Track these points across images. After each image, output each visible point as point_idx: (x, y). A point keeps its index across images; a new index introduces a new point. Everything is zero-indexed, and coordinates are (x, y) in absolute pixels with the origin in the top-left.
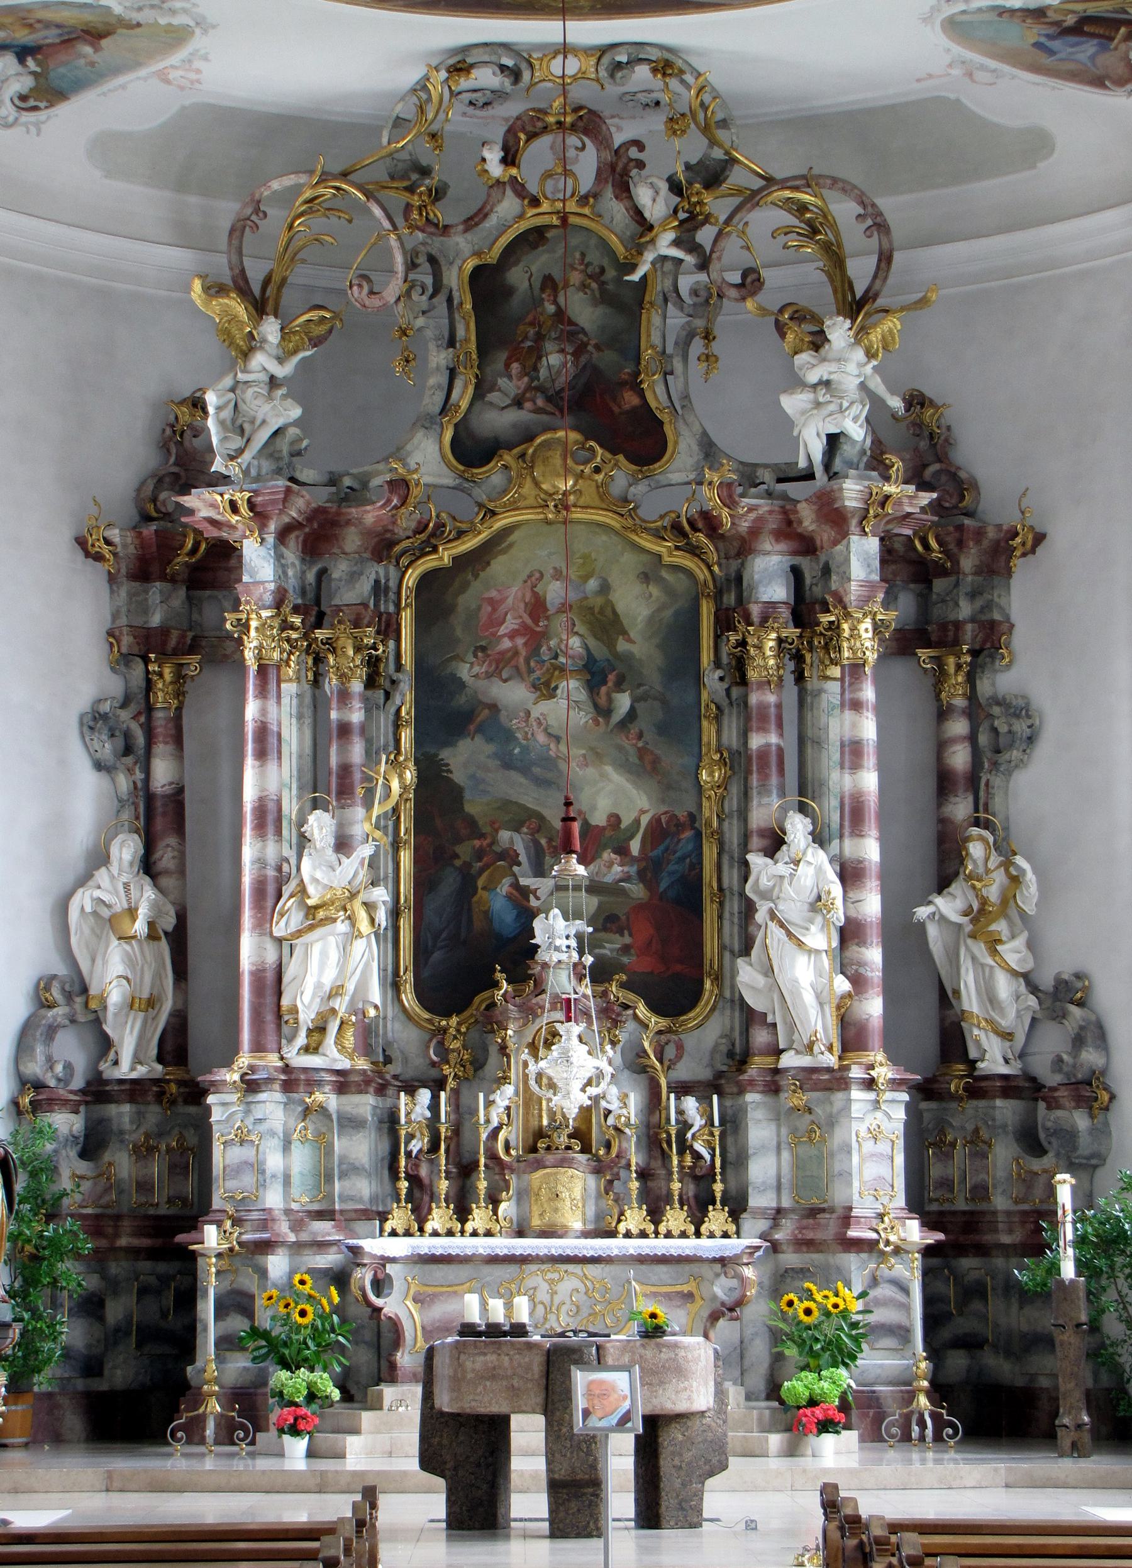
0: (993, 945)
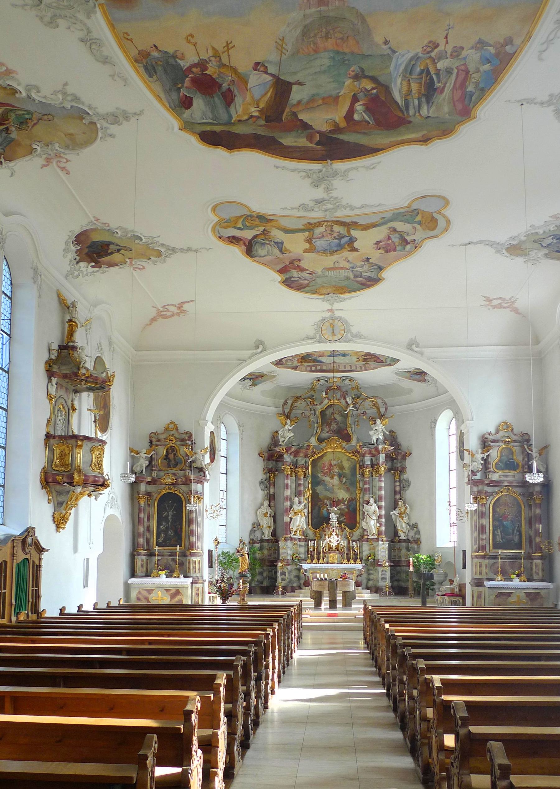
0: (402, 518)
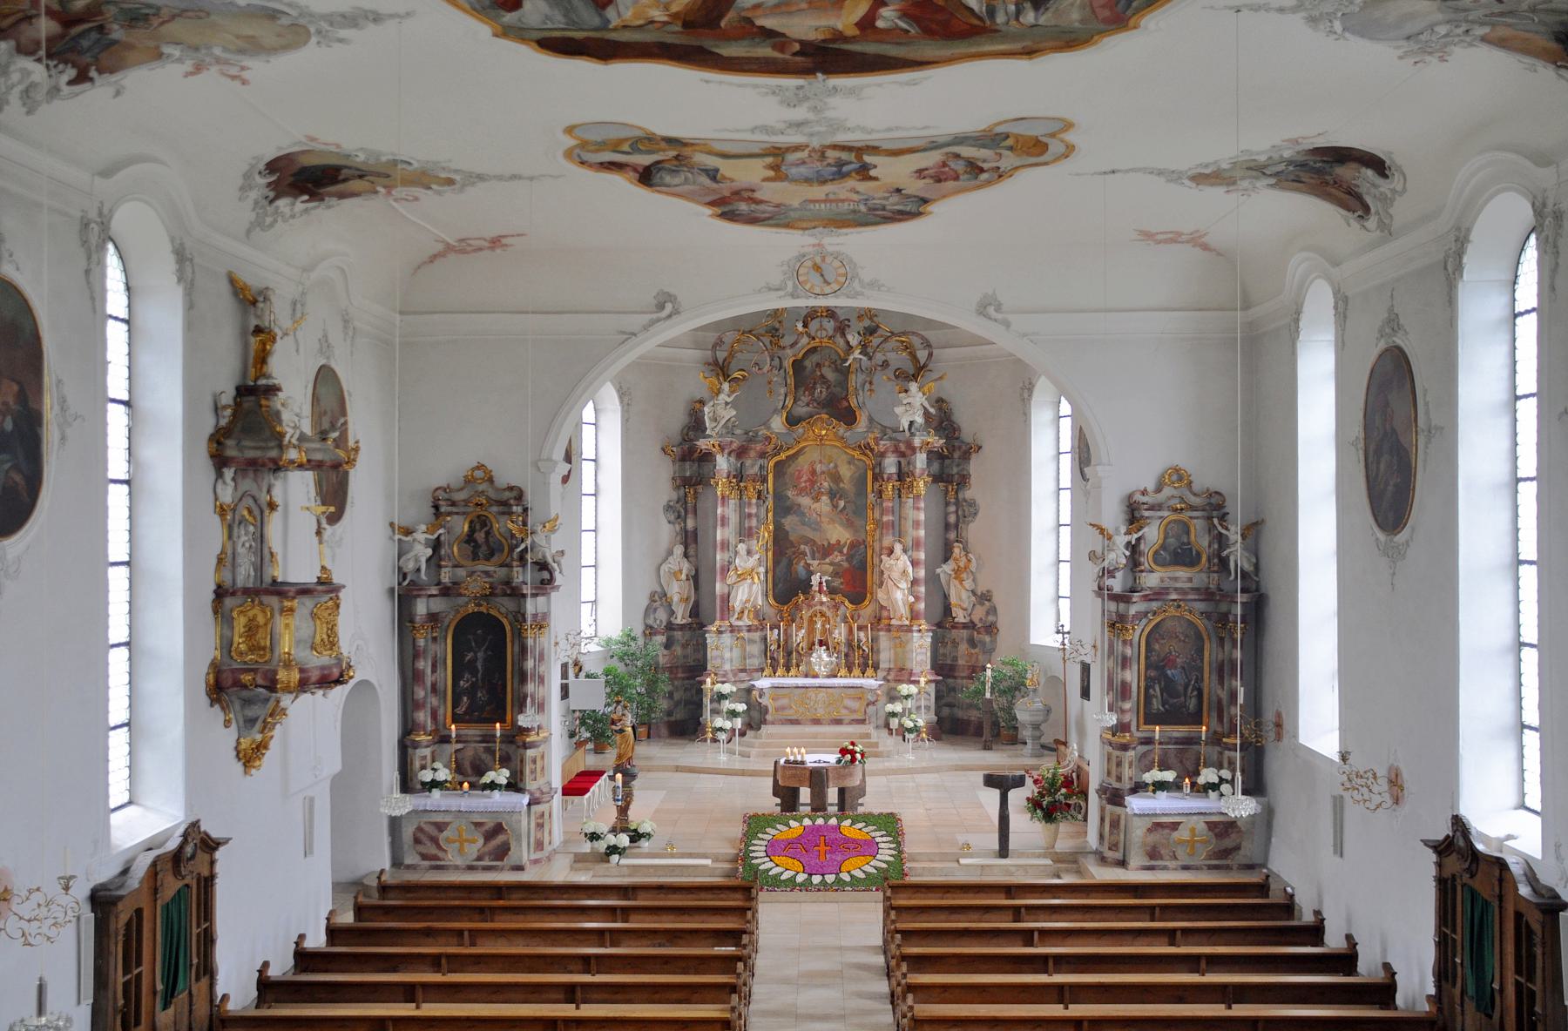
0: (961, 581)
